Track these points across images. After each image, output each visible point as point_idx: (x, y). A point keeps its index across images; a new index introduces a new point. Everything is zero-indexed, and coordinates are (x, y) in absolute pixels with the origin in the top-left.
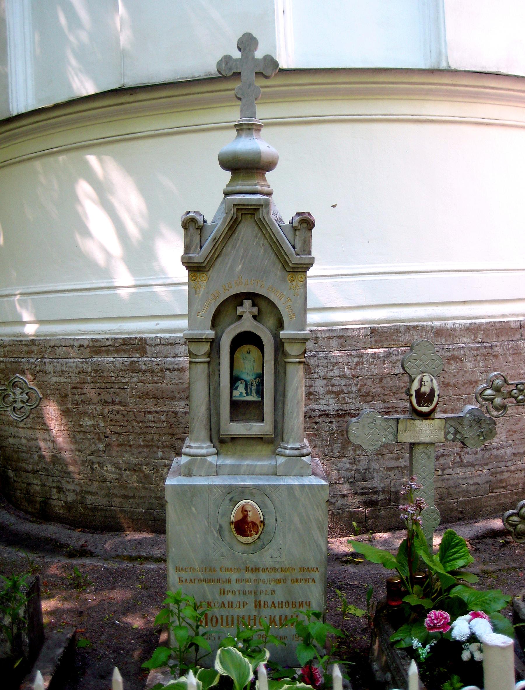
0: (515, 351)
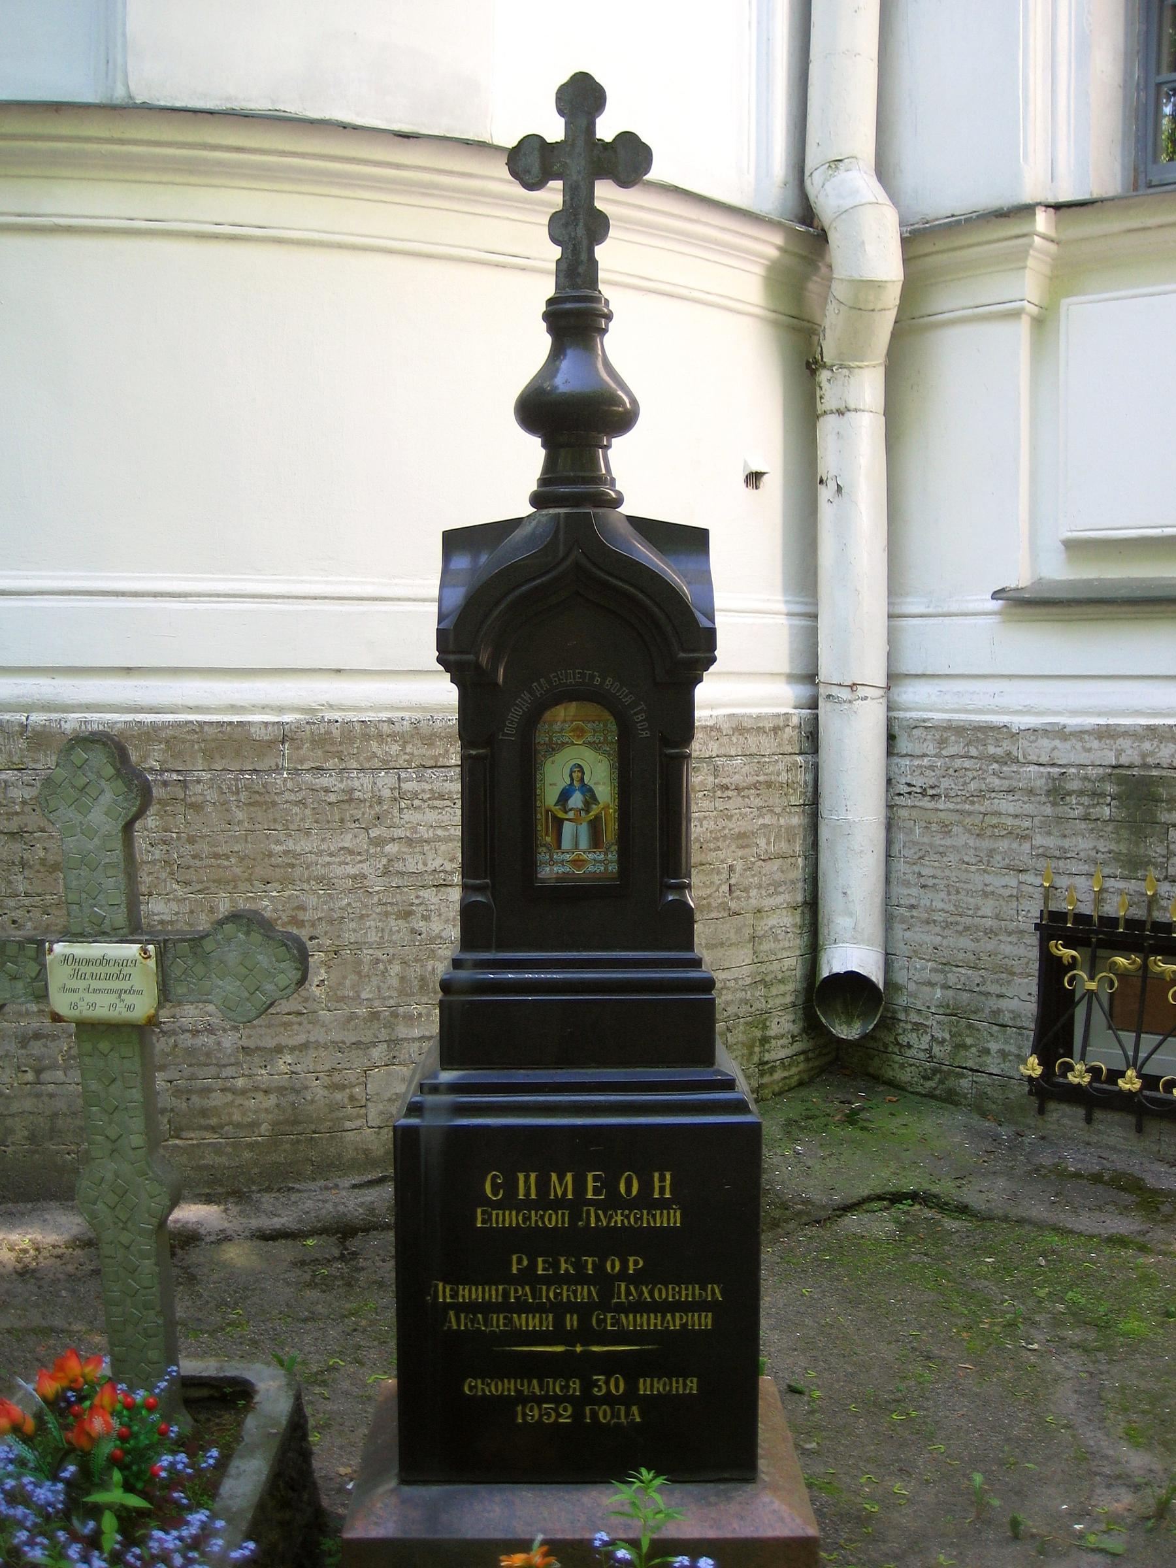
0: (257, 797)
